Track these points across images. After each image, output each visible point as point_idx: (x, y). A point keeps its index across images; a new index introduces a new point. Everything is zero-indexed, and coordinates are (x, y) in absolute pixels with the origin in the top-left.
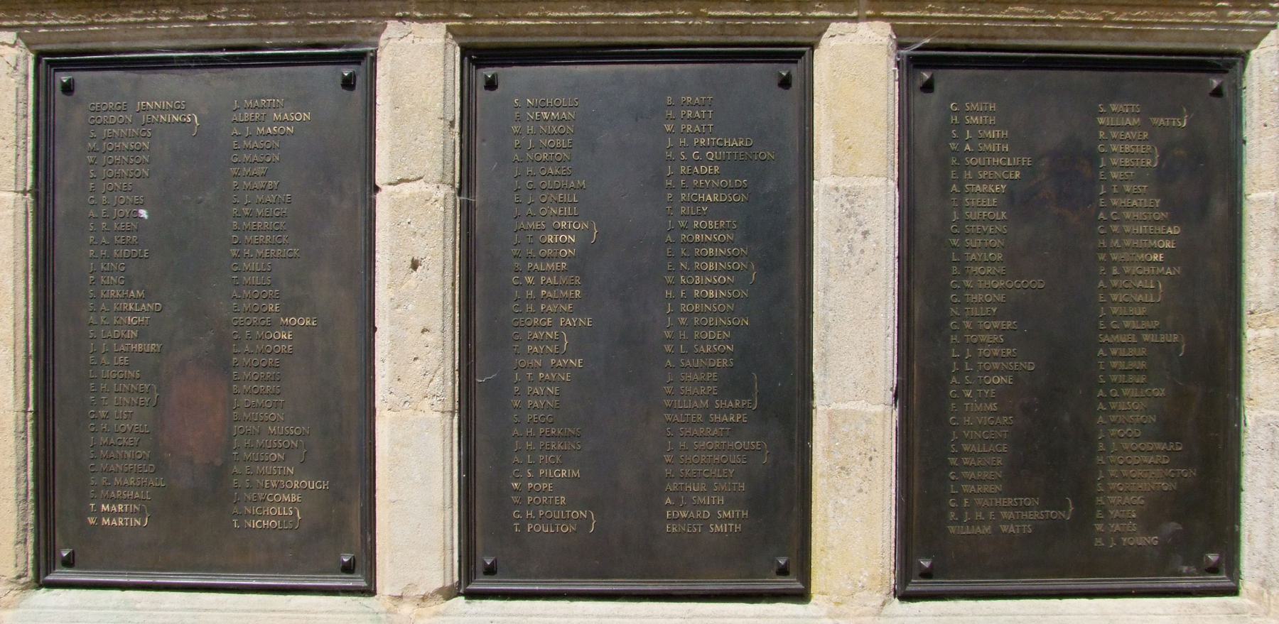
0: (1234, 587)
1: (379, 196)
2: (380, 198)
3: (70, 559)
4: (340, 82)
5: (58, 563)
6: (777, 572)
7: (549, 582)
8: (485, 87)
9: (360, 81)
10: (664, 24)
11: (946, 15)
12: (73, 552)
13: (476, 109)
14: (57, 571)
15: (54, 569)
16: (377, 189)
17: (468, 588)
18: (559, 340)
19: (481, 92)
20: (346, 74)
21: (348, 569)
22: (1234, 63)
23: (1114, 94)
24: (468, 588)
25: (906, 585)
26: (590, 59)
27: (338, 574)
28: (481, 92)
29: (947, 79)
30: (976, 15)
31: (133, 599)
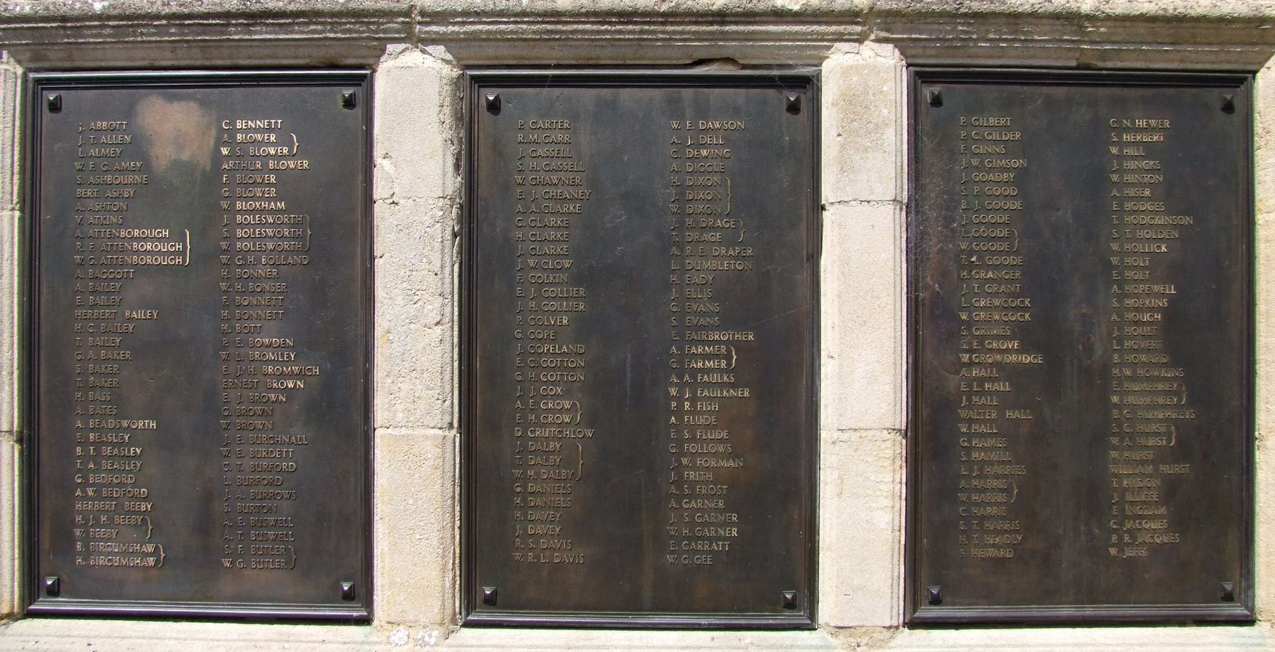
0: (1247, 616)
1: (825, 214)
2: (827, 216)
3: (351, 591)
4: (785, 107)
5: (43, 591)
6: (929, 602)
7: (559, 614)
8: (50, 109)
9: (804, 106)
10: (1131, 50)
11: (320, 36)
12: (59, 579)
13: (41, 131)
14: (41, 599)
15: (38, 598)
16: (823, 208)
17: (469, 618)
18: (728, 357)
19: (47, 115)
20: (792, 99)
21: (349, 597)
22: (1246, 79)
23: (978, 108)
24: (469, 618)
25: (915, 611)
26: (1079, 80)
27: (340, 603)
28: (47, 115)
29: (956, 94)
30: (154, 39)
31: (198, 630)
